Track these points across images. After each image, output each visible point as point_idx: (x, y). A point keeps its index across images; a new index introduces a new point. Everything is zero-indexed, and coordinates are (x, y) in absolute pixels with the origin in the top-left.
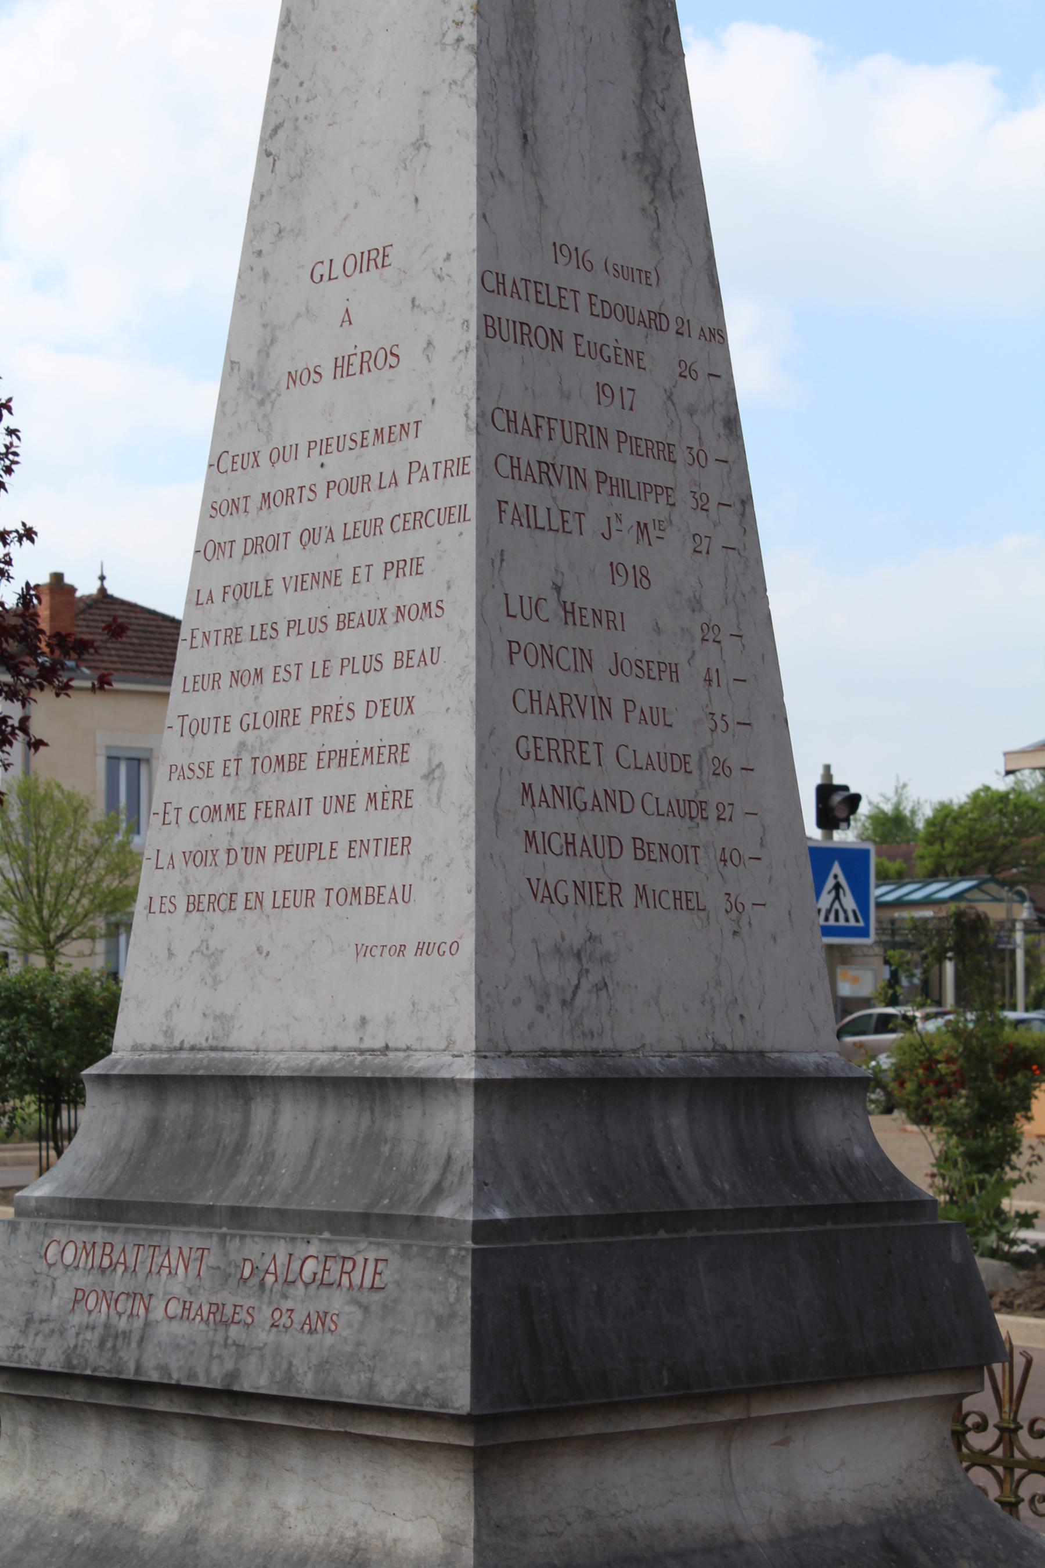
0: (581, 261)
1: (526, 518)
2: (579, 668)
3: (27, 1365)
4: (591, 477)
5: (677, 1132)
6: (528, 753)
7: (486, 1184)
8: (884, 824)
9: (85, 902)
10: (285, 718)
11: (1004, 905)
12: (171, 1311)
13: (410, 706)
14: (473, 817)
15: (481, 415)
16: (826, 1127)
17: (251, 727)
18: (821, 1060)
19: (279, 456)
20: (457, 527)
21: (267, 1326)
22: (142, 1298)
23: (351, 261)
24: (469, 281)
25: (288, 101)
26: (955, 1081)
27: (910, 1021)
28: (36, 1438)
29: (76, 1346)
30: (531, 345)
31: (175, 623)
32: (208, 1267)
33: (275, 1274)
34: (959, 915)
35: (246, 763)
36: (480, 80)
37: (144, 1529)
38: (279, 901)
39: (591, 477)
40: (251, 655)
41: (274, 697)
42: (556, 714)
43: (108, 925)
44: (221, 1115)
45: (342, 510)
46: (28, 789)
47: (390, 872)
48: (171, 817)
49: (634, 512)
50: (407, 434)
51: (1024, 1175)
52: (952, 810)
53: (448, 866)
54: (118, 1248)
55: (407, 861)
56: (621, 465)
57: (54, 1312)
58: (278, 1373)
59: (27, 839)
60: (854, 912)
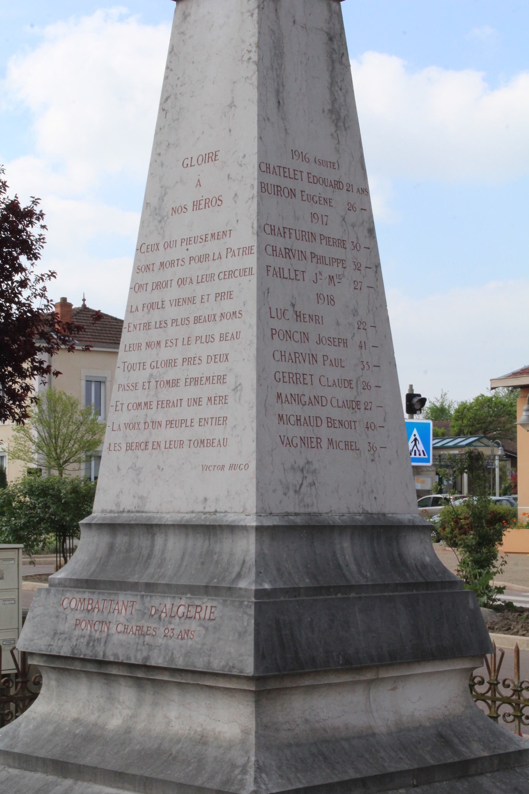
0: (304, 158)
1: (279, 273)
2: (303, 341)
3: (54, 653)
4: (308, 255)
5: (346, 549)
6: (280, 379)
7: (261, 573)
8: (436, 412)
9: (76, 446)
10: (170, 363)
11: (490, 448)
12: (119, 630)
13: (227, 358)
14: (255, 408)
15: (259, 227)
16: (414, 548)
17: (155, 367)
18: (411, 518)
19: (168, 245)
20: (248, 278)
21: (162, 636)
22: (106, 623)
23: (201, 158)
24: (254, 167)
25: (172, 86)
26: (468, 527)
27: (447, 500)
28: (58, 686)
29: (76, 645)
30: (281, 196)
31: (122, 321)
32: (136, 610)
33: (166, 613)
34: (470, 453)
35: (153, 383)
36: (259, 77)
37: (107, 727)
38: (168, 446)
39: (308, 255)
40: (155, 335)
41: (165, 353)
42: (292, 362)
43: (87, 456)
44: (142, 541)
45: (196, 270)
46: (51, 395)
47: (217, 432)
48: (119, 408)
49: (327, 270)
50: (226, 235)
51: (499, 570)
52: (467, 406)
53: (244, 430)
54: (95, 601)
55: (225, 428)
56: (321, 249)
57: (66, 630)
58: (167, 657)
59: (50, 417)
60: (423, 451)
